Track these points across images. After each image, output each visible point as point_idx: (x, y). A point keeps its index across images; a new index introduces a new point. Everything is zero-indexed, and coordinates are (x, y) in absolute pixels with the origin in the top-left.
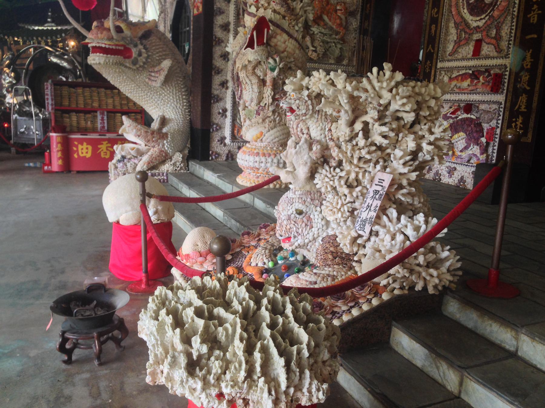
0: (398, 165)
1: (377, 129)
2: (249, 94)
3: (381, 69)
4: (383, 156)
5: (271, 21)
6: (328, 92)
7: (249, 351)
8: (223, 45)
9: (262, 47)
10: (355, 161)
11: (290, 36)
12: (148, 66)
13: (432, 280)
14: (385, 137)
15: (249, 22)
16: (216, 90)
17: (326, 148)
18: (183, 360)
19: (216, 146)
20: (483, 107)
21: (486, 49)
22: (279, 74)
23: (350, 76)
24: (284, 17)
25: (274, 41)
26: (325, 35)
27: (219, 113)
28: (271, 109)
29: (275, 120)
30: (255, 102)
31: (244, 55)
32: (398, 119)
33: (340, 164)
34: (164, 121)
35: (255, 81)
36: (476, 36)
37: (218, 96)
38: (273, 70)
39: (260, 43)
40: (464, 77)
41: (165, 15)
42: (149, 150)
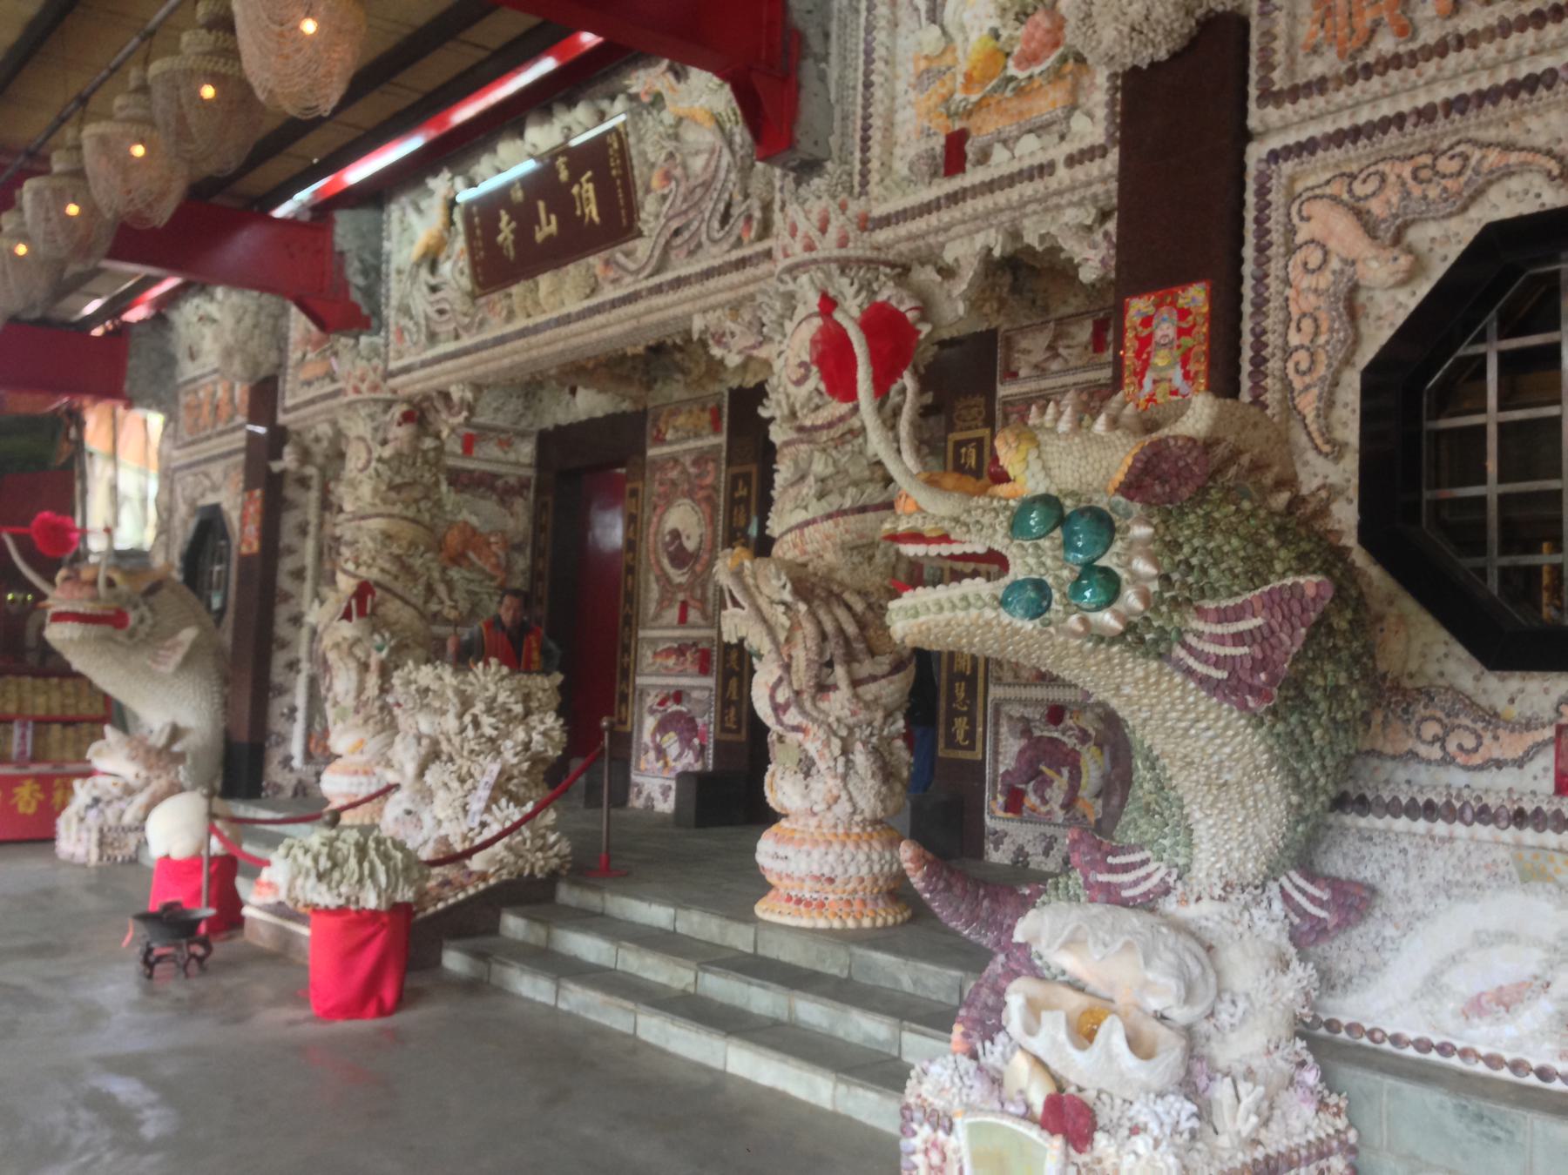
0: (509, 756)
1: (486, 721)
2: (342, 683)
3: (487, 663)
4: (493, 745)
5: (378, 584)
6: (435, 686)
7: (360, 863)
8: (293, 602)
9: (365, 620)
10: (465, 753)
11: (406, 602)
12: (155, 638)
13: (539, 863)
14: (496, 729)
15: (346, 584)
16: (278, 675)
17: (435, 743)
18: (313, 873)
19: (275, 773)
20: (695, 694)
21: (693, 615)
22: (390, 654)
23: (456, 671)
24: (396, 578)
25: (381, 610)
26: (471, 581)
27: (283, 715)
28: (377, 704)
29: (383, 721)
30: (353, 694)
31: (336, 629)
32: (509, 711)
33: (451, 759)
34: (176, 733)
35: (353, 665)
36: (681, 596)
37: (281, 685)
38: (380, 649)
39: (362, 613)
40: (668, 652)
41: (169, 539)
42: (148, 782)
